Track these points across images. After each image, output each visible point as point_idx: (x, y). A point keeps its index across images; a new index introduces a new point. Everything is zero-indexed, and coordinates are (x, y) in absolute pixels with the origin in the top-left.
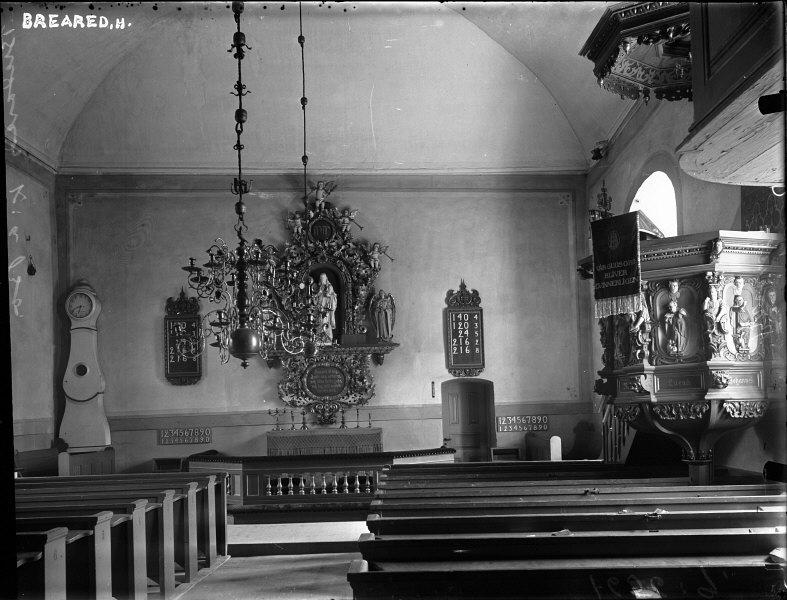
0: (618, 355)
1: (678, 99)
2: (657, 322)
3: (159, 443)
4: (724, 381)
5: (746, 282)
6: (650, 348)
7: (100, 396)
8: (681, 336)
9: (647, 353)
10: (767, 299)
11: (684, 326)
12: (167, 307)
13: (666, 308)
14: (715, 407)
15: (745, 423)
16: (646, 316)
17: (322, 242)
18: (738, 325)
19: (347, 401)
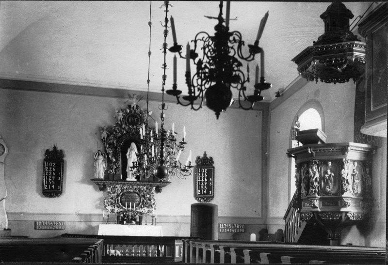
0: (303, 191)
1: (330, 82)
2: (322, 178)
3: (35, 229)
4: (349, 204)
5: (358, 164)
6: (318, 189)
7: (4, 200)
8: (331, 184)
9: (317, 190)
10: (366, 171)
11: (333, 180)
12: (46, 154)
13: (326, 173)
14: (344, 215)
15: (354, 223)
16: (317, 175)
17: (133, 126)
18: (354, 181)
19: (141, 211)
